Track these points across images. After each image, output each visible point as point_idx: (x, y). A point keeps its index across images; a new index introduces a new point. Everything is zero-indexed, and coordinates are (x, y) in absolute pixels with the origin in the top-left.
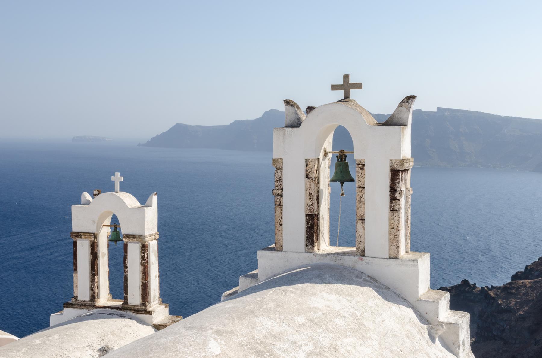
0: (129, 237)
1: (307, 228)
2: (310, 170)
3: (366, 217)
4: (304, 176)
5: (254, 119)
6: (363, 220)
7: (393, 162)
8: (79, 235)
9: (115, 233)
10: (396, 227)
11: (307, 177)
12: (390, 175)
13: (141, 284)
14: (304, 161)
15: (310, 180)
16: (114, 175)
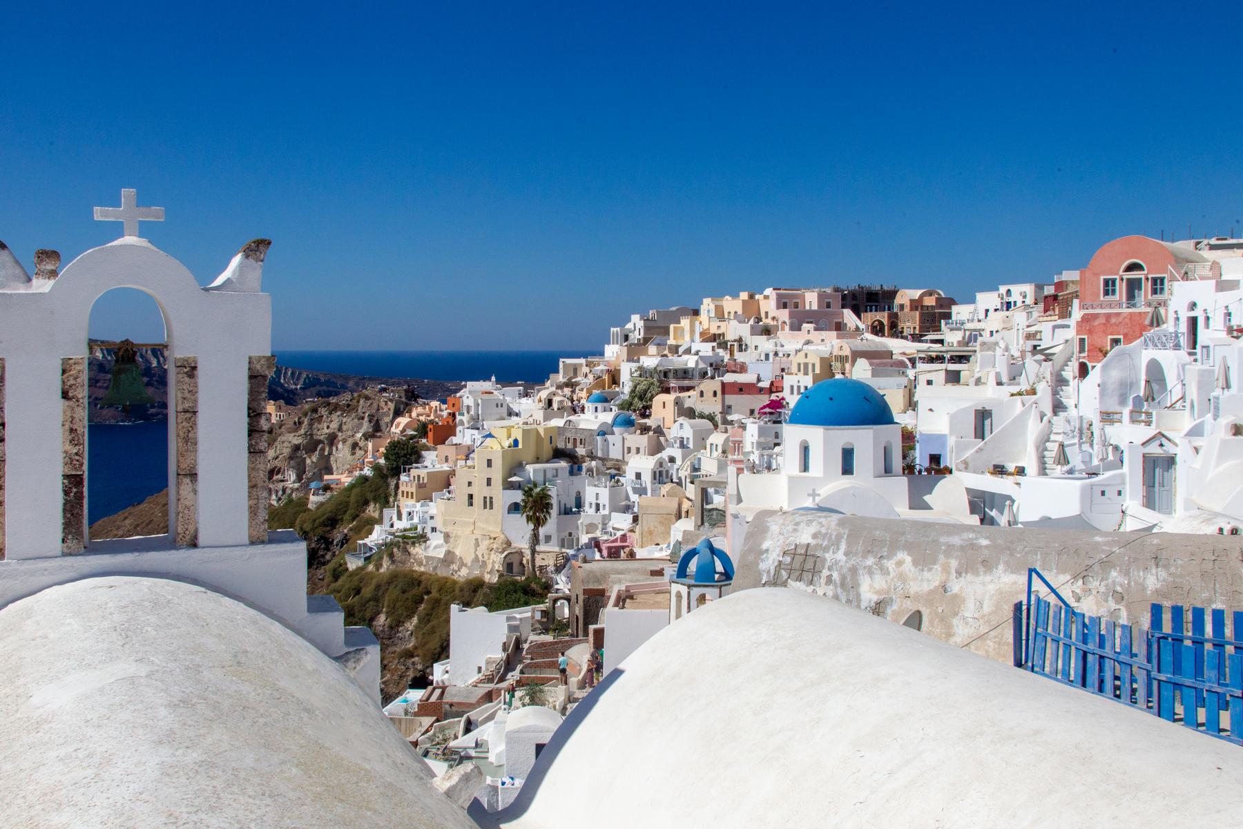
1: (65, 504)
2: (72, 382)
11: (65, 395)
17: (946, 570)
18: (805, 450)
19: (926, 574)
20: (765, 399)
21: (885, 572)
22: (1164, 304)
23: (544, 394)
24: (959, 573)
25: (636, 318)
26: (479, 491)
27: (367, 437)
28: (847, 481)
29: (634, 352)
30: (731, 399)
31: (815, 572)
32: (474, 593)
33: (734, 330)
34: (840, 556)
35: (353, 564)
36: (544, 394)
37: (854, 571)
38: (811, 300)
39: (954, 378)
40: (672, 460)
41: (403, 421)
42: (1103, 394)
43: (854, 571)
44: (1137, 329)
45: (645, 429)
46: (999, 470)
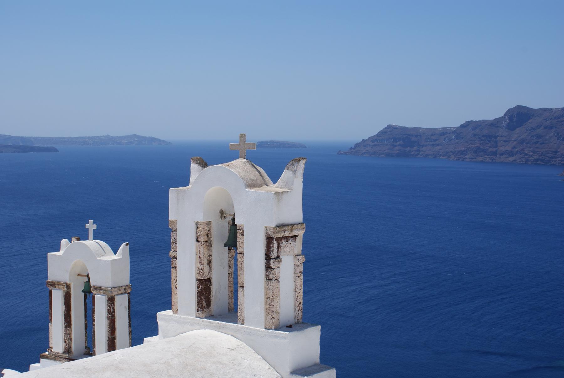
0: (96, 289)
3: (245, 285)
4: (194, 239)
5: (493, 119)
6: (243, 287)
7: (268, 229)
8: (53, 284)
9: (88, 283)
10: (271, 297)
11: (197, 241)
12: (266, 243)
13: (107, 339)
14: (194, 224)
15: (199, 244)
16: (94, 223)
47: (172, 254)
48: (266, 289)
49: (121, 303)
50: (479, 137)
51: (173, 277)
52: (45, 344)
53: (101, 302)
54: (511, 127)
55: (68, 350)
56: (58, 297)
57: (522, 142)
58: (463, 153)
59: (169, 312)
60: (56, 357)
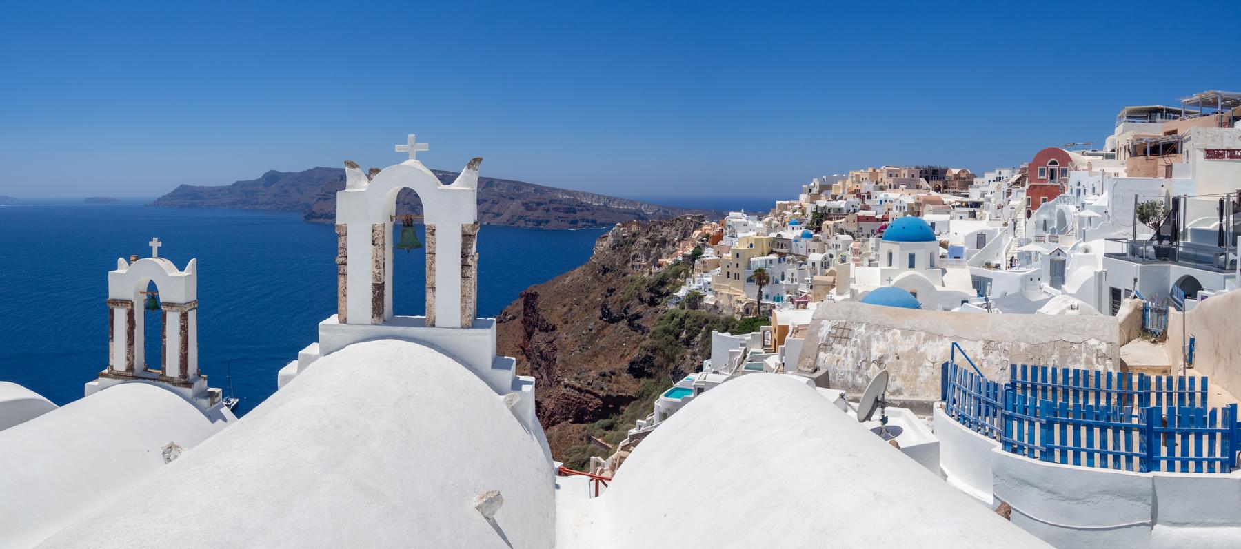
3: (437, 286)
8: (117, 302)
11: (373, 243)
17: (918, 339)
18: (891, 255)
19: (908, 341)
20: (878, 226)
21: (886, 339)
22: (1066, 181)
23: (767, 220)
24: (925, 340)
25: (815, 180)
26: (733, 270)
27: (679, 241)
28: (911, 272)
29: (814, 198)
30: (862, 224)
31: (848, 338)
32: (728, 326)
33: (866, 187)
34: (862, 329)
35: (671, 307)
36: (767, 220)
37: (869, 338)
38: (905, 174)
39: (973, 215)
40: (831, 256)
41: (697, 232)
42: (1037, 227)
43: (869, 338)
44: (1053, 193)
45: (817, 240)
46: (988, 265)
47: (338, 260)
48: (463, 287)
49: (192, 317)
50: (244, 193)
51: (341, 284)
52: (105, 363)
53: (173, 320)
54: (267, 185)
55: (131, 368)
56: (120, 315)
57: (275, 195)
58: (234, 203)
59: (334, 320)
60: (118, 375)
